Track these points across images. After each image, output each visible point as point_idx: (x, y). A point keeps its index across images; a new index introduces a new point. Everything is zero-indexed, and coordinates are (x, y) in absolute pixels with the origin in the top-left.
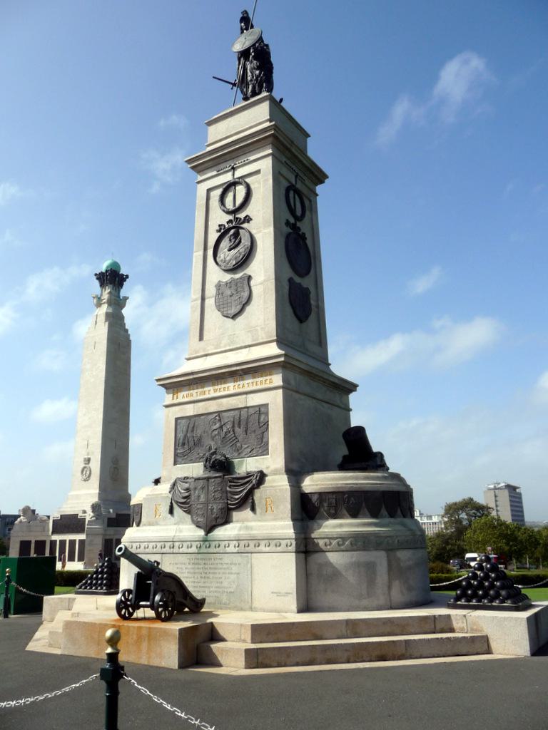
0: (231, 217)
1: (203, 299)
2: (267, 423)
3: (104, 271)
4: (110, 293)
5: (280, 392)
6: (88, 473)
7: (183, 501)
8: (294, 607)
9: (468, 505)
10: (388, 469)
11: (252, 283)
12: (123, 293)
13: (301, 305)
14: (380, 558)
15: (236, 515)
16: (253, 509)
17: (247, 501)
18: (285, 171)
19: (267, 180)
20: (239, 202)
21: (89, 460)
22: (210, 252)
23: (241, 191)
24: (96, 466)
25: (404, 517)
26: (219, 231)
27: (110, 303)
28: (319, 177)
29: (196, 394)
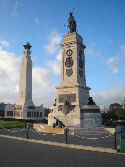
0: (68, 57)
1: (63, 72)
2: (76, 97)
3: (26, 45)
4: (27, 51)
5: (78, 91)
6: (68, 53)
7: (60, 108)
8: (80, 127)
9: (117, 104)
10: (95, 104)
11: (73, 70)
12: (30, 50)
13: (81, 74)
14: (94, 119)
15: (70, 112)
16: (73, 111)
17: (72, 109)
18: (79, 48)
19: (76, 51)
20: (70, 54)
21: (23, 92)
22: (65, 63)
23: (70, 51)
24: (24, 94)
25: (98, 113)
26: (66, 59)
27: (27, 53)
28: (85, 47)
29: (62, 90)
